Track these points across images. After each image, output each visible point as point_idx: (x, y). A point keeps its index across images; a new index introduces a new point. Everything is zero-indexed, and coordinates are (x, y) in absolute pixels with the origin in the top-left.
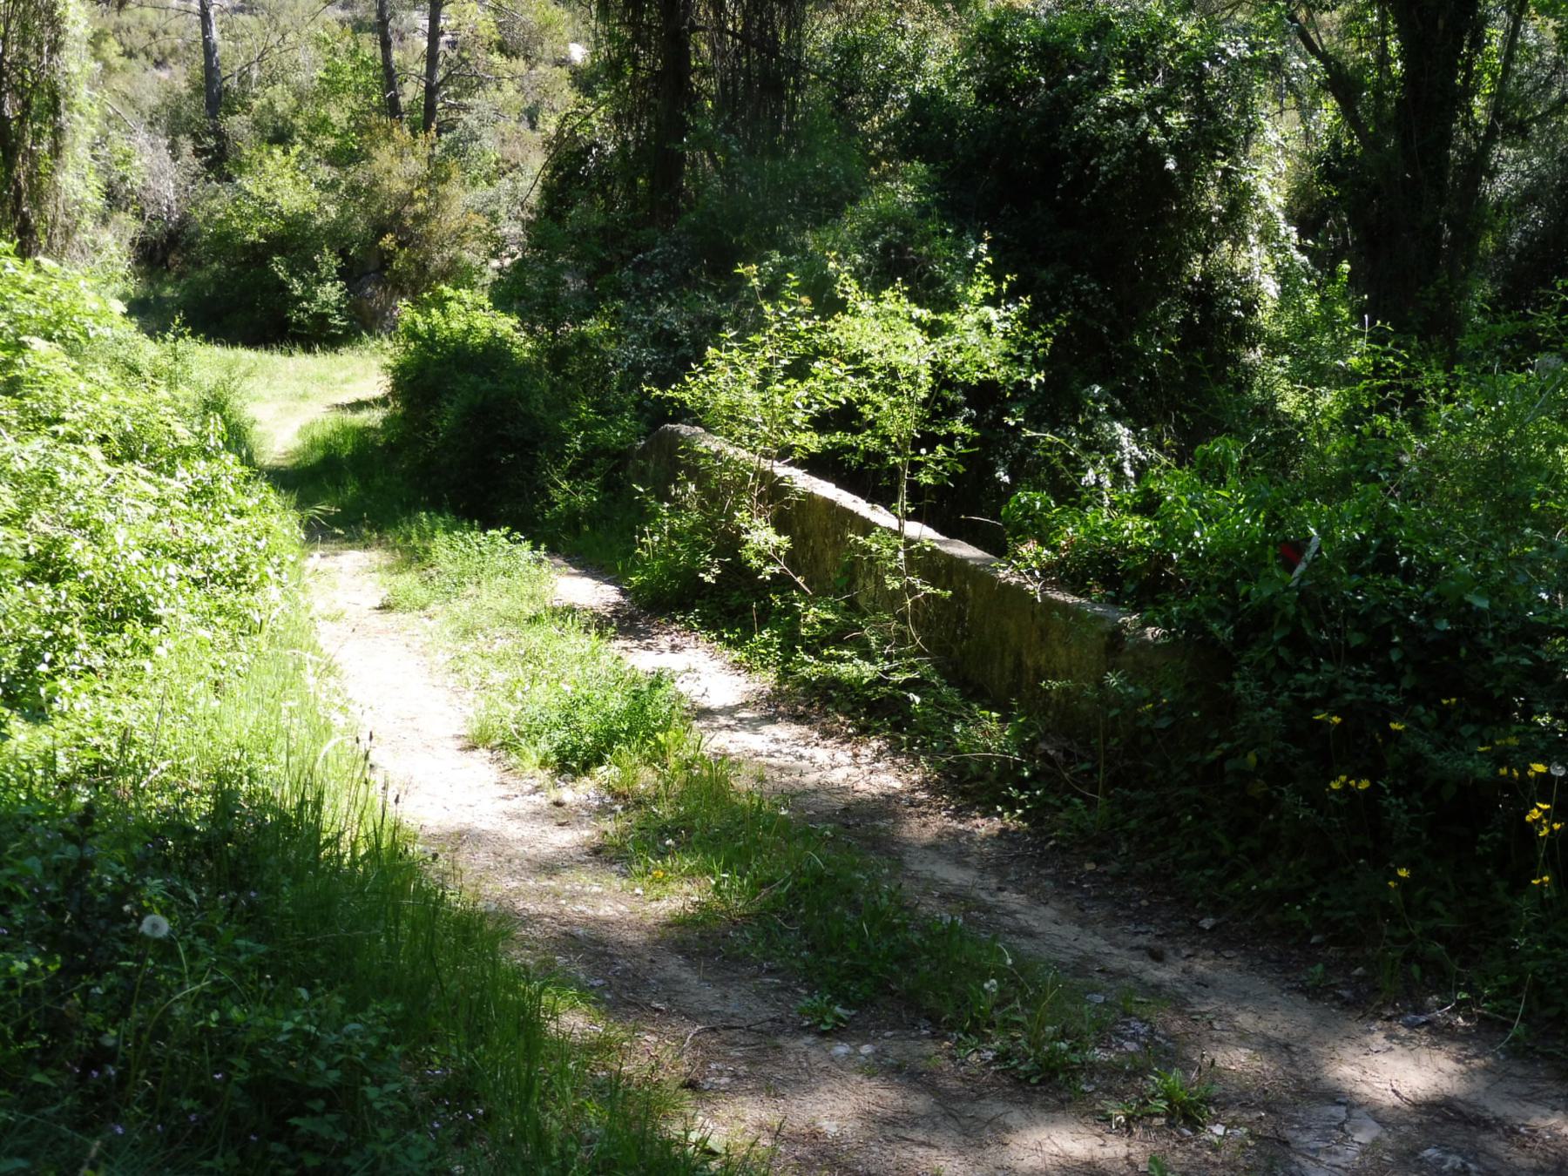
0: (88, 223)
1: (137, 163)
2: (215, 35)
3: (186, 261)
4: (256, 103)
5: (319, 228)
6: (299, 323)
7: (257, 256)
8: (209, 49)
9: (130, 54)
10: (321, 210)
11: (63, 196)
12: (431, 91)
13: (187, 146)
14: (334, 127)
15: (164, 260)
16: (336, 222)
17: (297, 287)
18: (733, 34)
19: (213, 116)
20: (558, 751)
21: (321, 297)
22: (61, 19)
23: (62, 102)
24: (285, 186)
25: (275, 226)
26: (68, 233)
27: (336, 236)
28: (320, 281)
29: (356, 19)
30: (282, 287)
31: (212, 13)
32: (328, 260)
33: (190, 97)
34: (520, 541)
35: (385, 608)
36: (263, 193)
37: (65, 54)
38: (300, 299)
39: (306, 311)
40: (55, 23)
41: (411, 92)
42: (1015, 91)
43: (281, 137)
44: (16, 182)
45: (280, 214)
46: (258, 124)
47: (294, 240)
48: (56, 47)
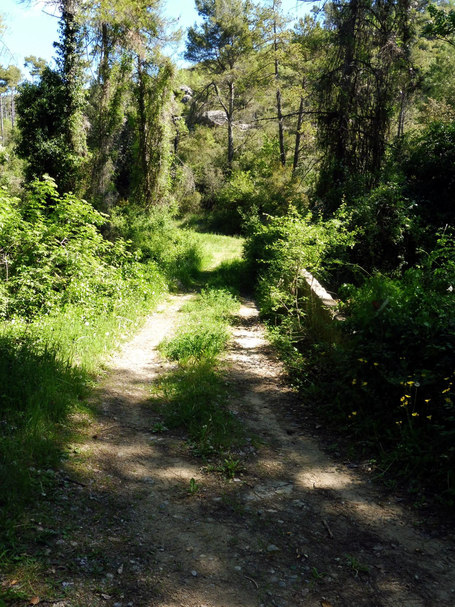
0: (167, 193)
1: (183, 175)
2: (233, 135)
3: (217, 208)
4: (241, 157)
5: (254, 197)
6: (244, 229)
7: (234, 206)
8: (230, 140)
9: (217, 142)
10: (254, 192)
11: (159, 185)
12: (297, 153)
13: (220, 171)
14: (266, 165)
15: (211, 207)
16: (259, 196)
17: (244, 217)
18: (360, 132)
19: (230, 161)
20: (173, 353)
21: (252, 220)
22: (162, 132)
23: (161, 156)
24: (243, 184)
25: (240, 197)
26: (160, 196)
27: (259, 201)
28: (252, 215)
29: (290, 130)
30: (240, 216)
31: (232, 128)
32: (255, 208)
33: (224, 155)
34: (229, 294)
35: (180, 311)
36: (237, 186)
37: (163, 142)
38: (245, 221)
39: (246, 224)
40: (160, 133)
41: (290, 154)
42: (133, 133)
43: (247, 168)
44: (147, 181)
45: (241, 193)
46: (241, 164)
47: (245, 201)
48: (160, 140)
